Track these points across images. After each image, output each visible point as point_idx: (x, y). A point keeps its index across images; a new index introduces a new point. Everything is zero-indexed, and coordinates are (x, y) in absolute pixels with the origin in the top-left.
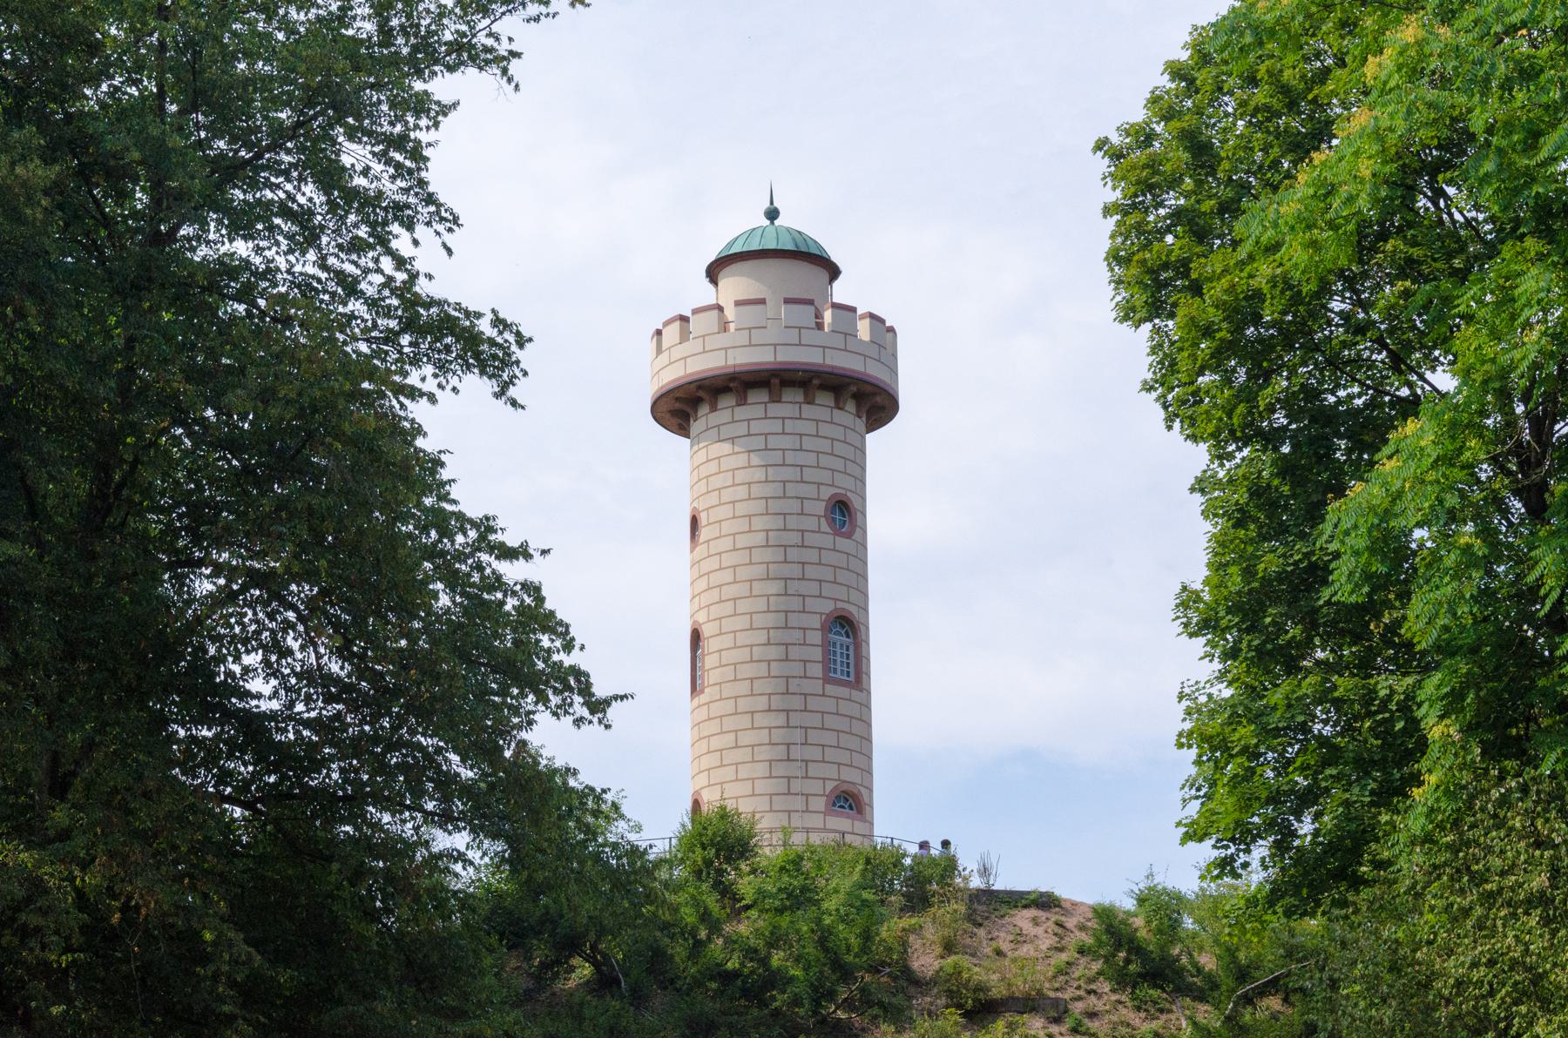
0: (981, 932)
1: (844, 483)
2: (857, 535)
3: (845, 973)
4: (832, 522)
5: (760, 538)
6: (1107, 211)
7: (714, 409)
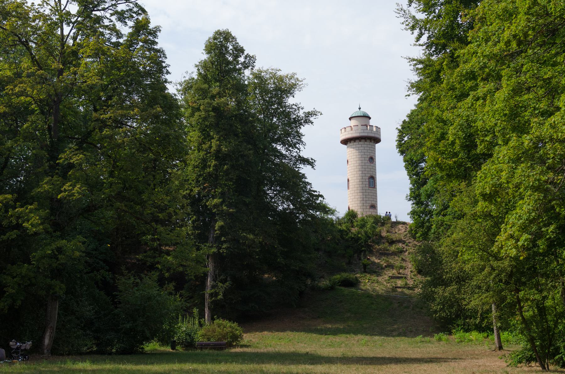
0: (393, 229)
1: (372, 154)
2: (374, 163)
3: (370, 238)
4: (370, 161)
5: (358, 164)
6: (396, 141)
7: (350, 143)
